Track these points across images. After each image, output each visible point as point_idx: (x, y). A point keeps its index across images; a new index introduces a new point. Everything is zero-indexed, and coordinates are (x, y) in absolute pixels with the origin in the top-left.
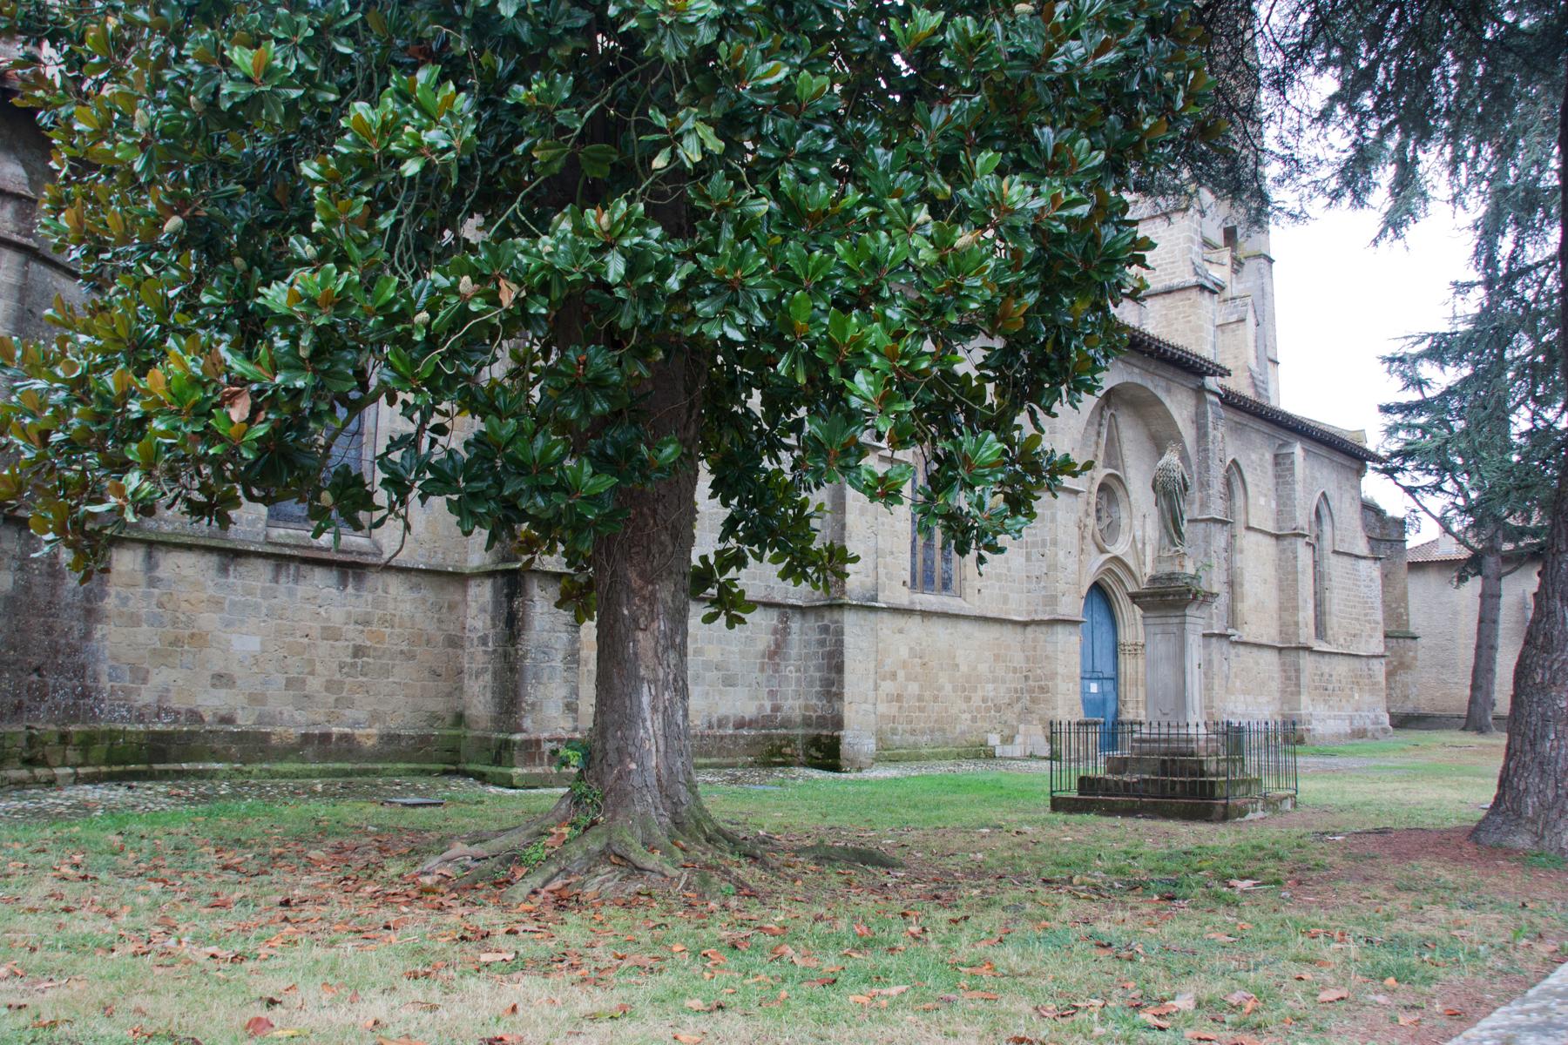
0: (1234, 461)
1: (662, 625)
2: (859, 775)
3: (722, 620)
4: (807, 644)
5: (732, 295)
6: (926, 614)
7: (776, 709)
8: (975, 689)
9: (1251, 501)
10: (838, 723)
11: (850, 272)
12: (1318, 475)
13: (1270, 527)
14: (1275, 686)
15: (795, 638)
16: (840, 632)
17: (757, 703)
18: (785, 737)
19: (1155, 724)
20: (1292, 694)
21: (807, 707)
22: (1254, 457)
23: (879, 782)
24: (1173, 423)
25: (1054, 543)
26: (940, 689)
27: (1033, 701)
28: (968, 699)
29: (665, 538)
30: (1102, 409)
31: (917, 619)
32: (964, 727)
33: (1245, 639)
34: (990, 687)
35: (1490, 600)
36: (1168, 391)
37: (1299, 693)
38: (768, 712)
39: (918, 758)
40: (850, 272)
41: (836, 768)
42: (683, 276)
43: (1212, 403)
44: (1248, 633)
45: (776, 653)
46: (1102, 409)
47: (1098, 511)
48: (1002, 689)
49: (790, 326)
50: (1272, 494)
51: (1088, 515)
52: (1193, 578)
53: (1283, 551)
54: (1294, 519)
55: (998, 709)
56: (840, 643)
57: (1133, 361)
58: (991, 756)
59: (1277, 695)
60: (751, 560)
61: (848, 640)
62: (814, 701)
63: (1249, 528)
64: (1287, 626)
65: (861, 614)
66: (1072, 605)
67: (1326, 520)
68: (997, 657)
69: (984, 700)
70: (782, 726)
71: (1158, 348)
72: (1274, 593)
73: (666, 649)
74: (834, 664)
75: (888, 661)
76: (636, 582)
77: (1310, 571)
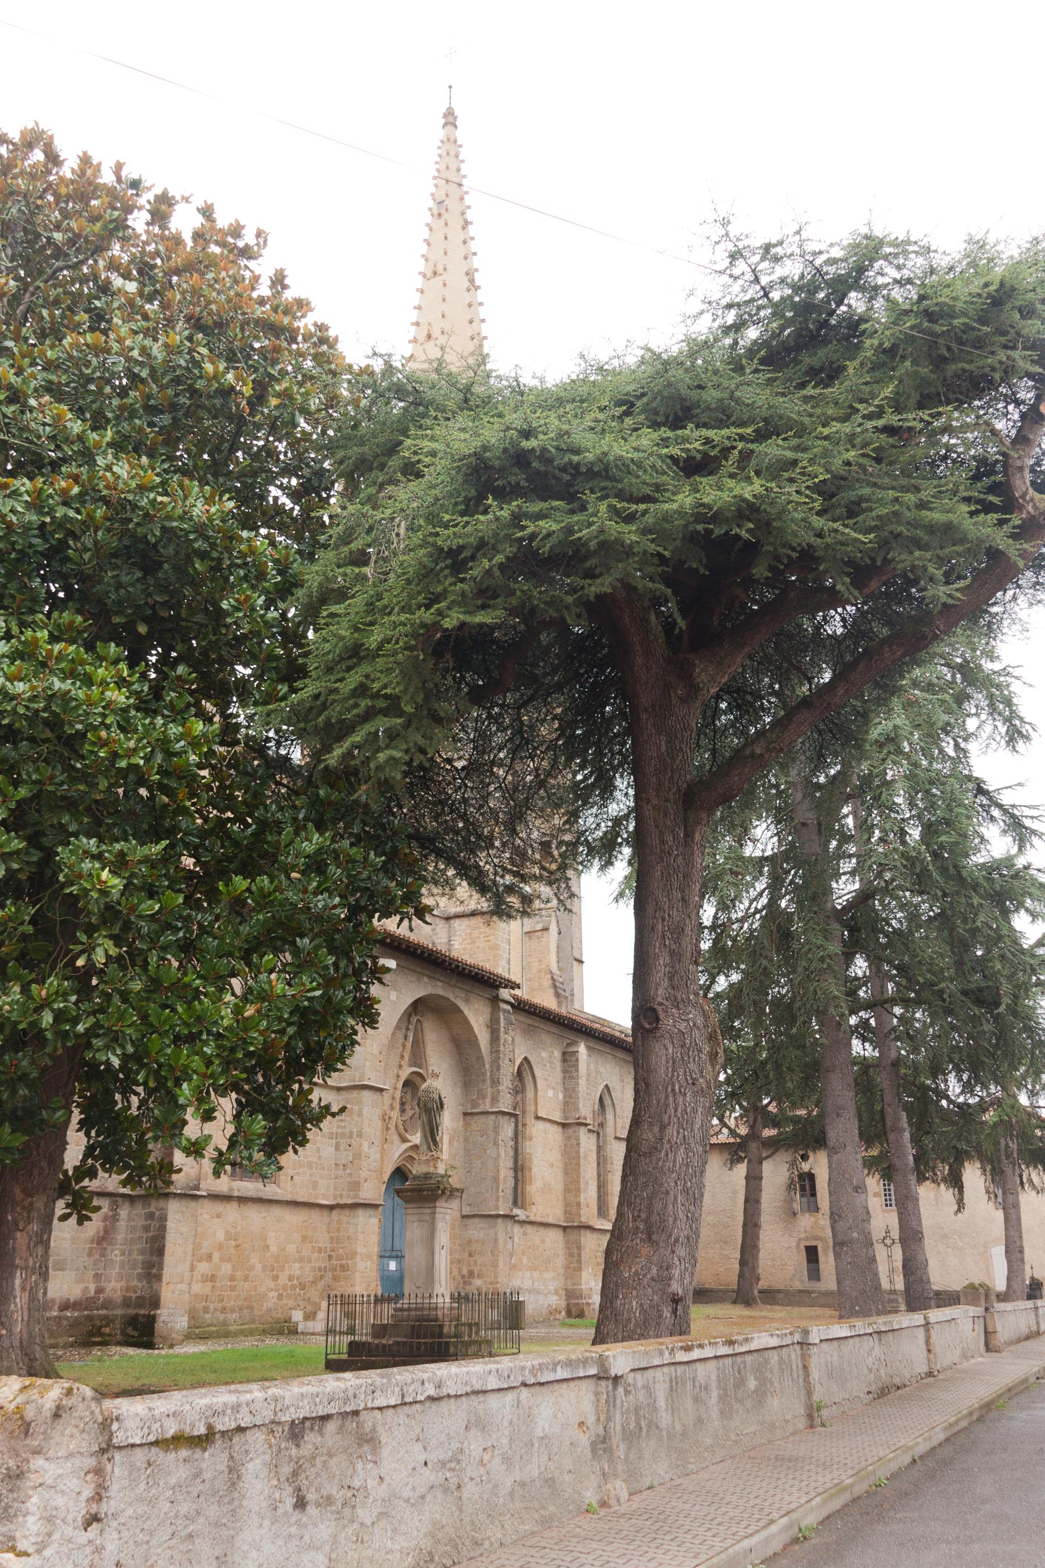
0: (526, 1059)
1: (35, 1227)
2: (171, 1351)
3: (73, 1220)
4: (133, 1229)
5: (115, 1039)
6: (243, 1200)
7: (99, 1291)
8: (282, 1269)
9: (540, 1093)
10: (155, 1303)
11: (187, 1025)
12: (602, 1069)
13: (557, 1117)
14: (560, 1262)
15: (122, 1224)
16: (164, 1219)
17: (82, 1286)
18: (106, 1317)
19: (413, 1296)
20: (574, 1270)
21: (127, 1289)
22: (544, 1054)
23: (186, 1356)
24: (470, 1028)
25: (360, 1135)
26: (251, 1268)
27: (335, 1279)
28: (276, 1278)
29: (44, 1164)
30: (410, 1015)
31: (235, 1205)
32: (270, 1305)
33: (532, 1218)
34: (297, 1266)
35: (754, 1180)
36: (467, 1001)
37: (580, 1269)
38: (92, 1293)
39: (227, 1335)
40: (187, 1025)
41: (150, 1345)
42: (87, 1025)
43: (505, 1011)
44: (537, 1212)
45: (104, 1239)
46: (410, 1015)
47: (402, 1104)
48: (308, 1268)
49: (148, 1054)
50: (560, 1087)
51: (392, 1108)
52: (442, 1176)
53: (568, 1138)
54: (577, 1109)
55: (303, 1287)
56: (163, 1228)
57: (437, 976)
58: (293, 1331)
59: (562, 1271)
60: (100, 1173)
61: (170, 1225)
62: (135, 1283)
63: (537, 1118)
64: (571, 1206)
65: (184, 1202)
66: (373, 1190)
67: (609, 1110)
68: (304, 1238)
69: (291, 1279)
70: (104, 1307)
71: (457, 967)
72: (560, 1176)
73: (36, 1245)
74: (156, 1248)
75: (205, 1244)
76: (18, 1194)
77: (593, 1156)
